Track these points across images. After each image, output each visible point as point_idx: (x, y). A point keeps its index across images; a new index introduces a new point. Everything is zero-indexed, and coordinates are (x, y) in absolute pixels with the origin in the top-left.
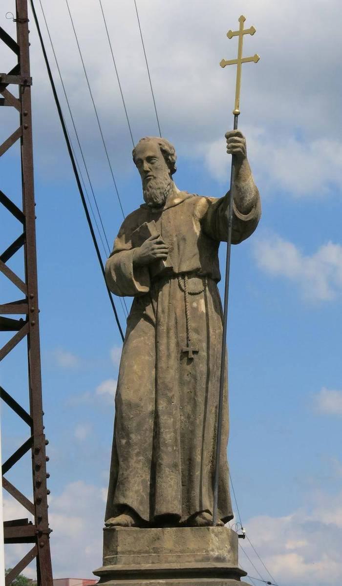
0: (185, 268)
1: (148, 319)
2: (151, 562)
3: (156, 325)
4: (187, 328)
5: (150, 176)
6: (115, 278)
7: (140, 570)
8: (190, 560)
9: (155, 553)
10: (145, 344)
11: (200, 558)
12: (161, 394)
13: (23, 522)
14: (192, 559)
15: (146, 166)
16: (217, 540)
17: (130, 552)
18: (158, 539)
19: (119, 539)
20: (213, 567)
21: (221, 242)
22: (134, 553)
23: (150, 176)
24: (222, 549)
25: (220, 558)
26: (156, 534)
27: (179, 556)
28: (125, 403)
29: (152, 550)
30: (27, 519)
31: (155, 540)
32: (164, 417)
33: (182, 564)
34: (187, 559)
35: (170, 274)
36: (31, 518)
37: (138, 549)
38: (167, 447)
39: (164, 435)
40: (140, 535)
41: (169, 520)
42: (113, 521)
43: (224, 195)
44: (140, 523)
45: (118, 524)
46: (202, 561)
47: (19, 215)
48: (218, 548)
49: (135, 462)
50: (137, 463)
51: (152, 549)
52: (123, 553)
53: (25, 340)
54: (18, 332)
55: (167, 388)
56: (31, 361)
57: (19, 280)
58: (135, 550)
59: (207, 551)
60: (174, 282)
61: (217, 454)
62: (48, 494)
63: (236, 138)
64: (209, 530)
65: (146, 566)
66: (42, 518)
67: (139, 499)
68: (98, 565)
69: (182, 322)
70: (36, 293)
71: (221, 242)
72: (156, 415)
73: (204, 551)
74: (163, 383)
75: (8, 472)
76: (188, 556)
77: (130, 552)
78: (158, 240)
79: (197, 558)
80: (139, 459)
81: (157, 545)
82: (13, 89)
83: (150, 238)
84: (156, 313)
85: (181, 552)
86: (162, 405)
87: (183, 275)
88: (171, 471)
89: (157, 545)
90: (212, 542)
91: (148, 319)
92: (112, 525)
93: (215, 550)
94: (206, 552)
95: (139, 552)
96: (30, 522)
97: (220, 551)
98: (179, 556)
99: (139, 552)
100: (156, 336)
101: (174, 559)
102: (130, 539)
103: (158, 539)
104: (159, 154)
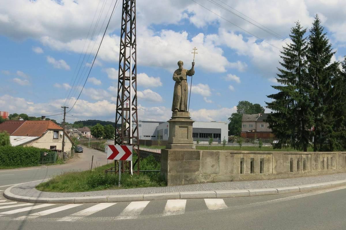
0: (185, 79)
1: (180, 85)
3: (181, 86)
4: (231, 7)
6: (313, 138)
21: (125, 153)
35: (183, 79)
44: (179, 111)
55: (183, 94)
57: (125, 69)
60: (183, 80)
61: (234, 149)
65: (181, 117)
66: (136, 108)
69: (185, 86)
71: (125, 153)
72: (181, 97)
75: (25, 114)
82: (122, 44)
86: (182, 96)
87: (185, 80)
91: (180, 85)
100: (181, 87)
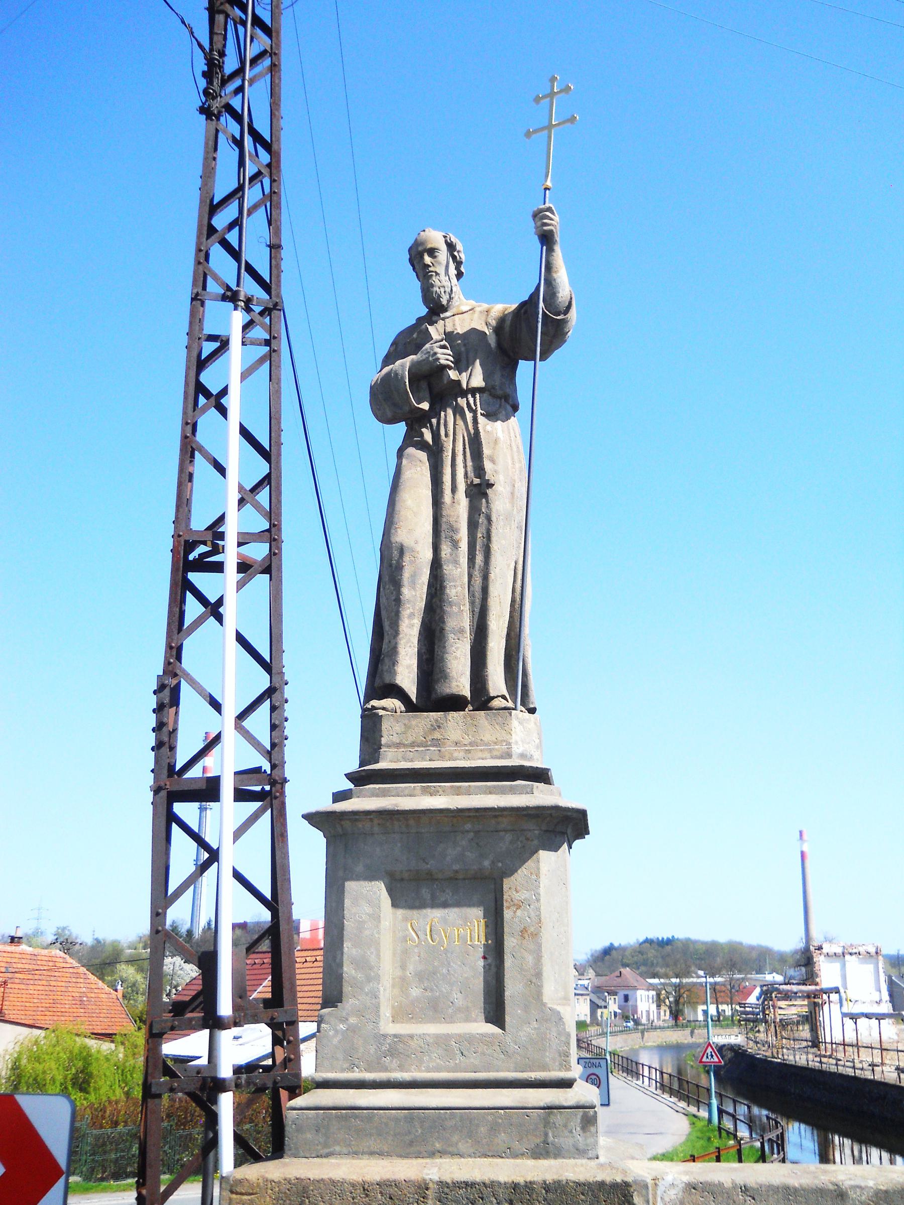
2: (428, 758)
5: (433, 272)
7: (414, 768)
8: (484, 756)
9: (433, 746)
10: (264, 1102)
11: (498, 754)
12: (444, 536)
13: (257, 770)
14: (487, 755)
15: (427, 259)
16: (522, 730)
17: (398, 745)
18: (439, 727)
19: (383, 727)
20: (518, 764)
22: (405, 746)
23: (433, 272)
24: (529, 743)
25: (526, 756)
26: (437, 721)
27: (468, 750)
28: (396, 546)
29: (429, 743)
30: (261, 767)
31: (435, 729)
32: (448, 566)
33: (472, 761)
34: (480, 755)
36: (266, 766)
37: (410, 740)
38: (451, 606)
39: (448, 591)
40: (414, 723)
41: (455, 703)
42: (374, 703)
43: (526, 298)
44: (411, 707)
45: (384, 709)
46: (501, 757)
47: (267, 667)
48: (522, 741)
49: (407, 626)
50: (410, 628)
51: (430, 741)
52: (389, 746)
53: (266, 819)
54: (261, 803)
56: (273, 594)
58: (406, 742)
59: (509, 744)
62: (286, 739)
63: (548, 213)
64: (511, 715)
67: (412, 676)
68: (353, 765)
70: (280, 521)
73: (504, 744)
74: (448, 523)
76: (481, 750)
77: (398, 745)
78: (442, 343)
79: (495, 753)
80: (412, 622)
81: (437, 735)
83: (431, 342)
84: (436, 435)
85: (471, 744)
88: (456, 638)
89: (437, 735)
90: (515, 732)
92: (374, 708)
93: (520, 743)
94: (506, 745)
95: (413, 745)
96: (265, 770)
97: (525, 745)
98: (469, 751)
99: (413, 745)
101: (462, 754)
102: (398, 728)
103: (439, 727)
104: (444, 248)
